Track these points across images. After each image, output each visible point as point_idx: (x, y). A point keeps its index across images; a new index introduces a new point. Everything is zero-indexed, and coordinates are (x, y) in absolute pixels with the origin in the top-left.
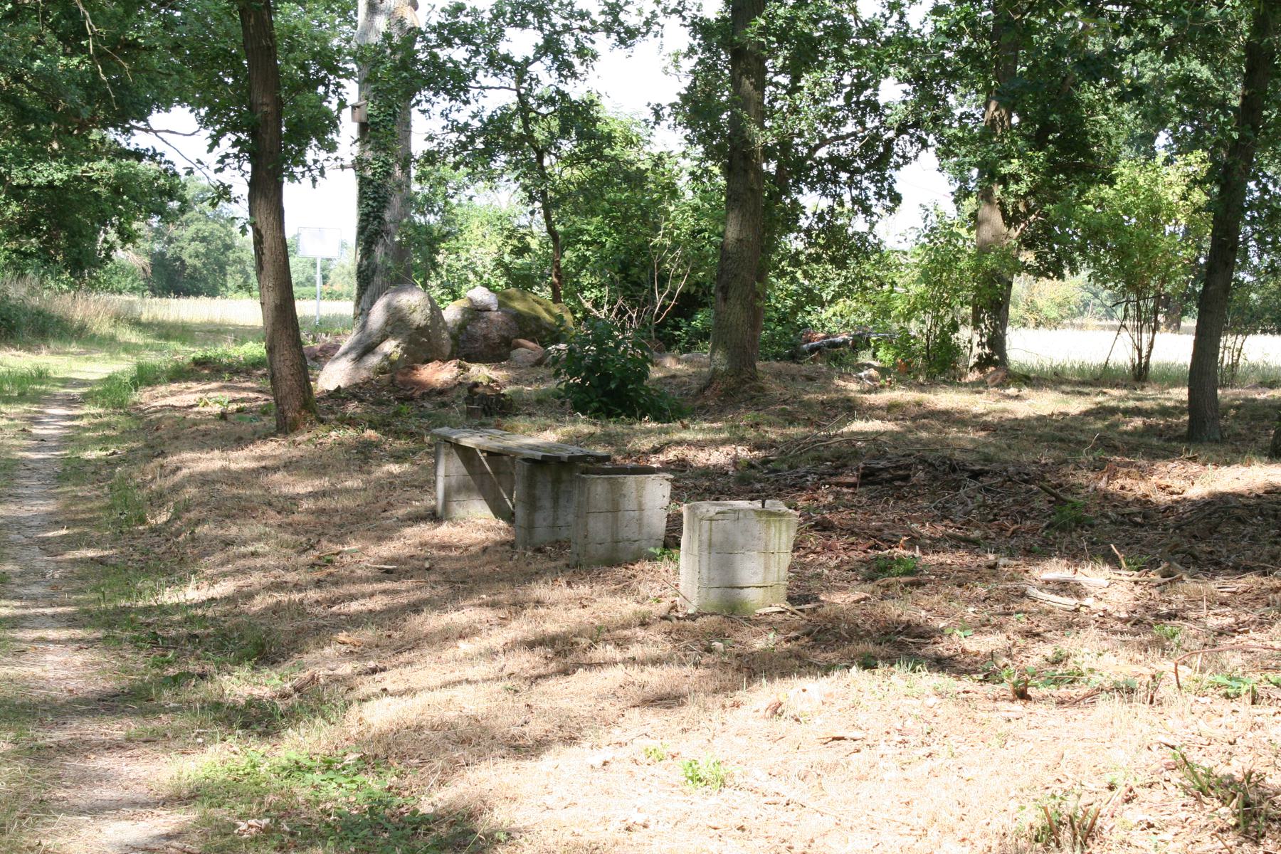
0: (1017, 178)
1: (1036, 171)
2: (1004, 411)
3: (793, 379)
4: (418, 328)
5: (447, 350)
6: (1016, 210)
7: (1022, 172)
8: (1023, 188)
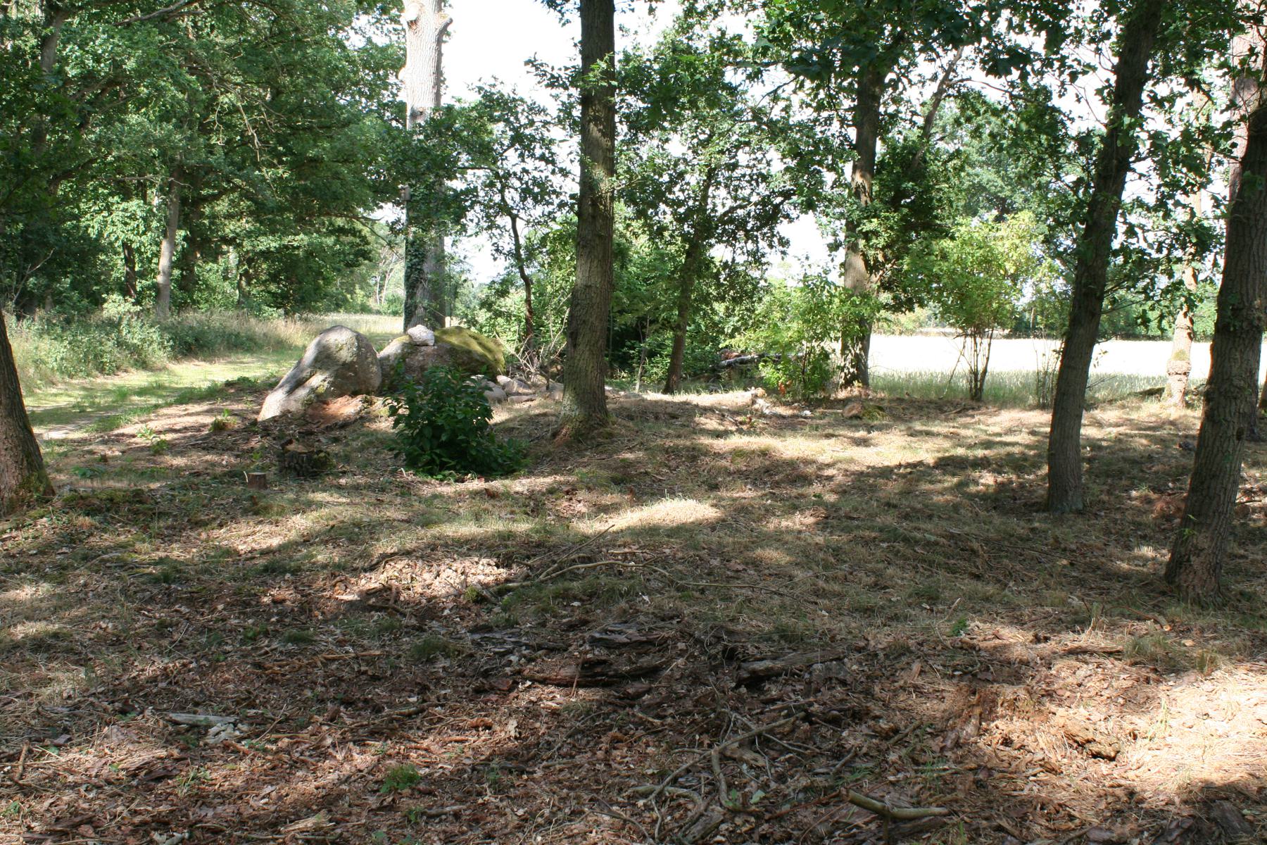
0: (876, 233)
1: (891, 228)
2: (851, 461)
3: (657, 418)
4: (344, 364)
5: (376, 382)
6: (876, 260)
7: (881, 229)
8: (881, 242)
